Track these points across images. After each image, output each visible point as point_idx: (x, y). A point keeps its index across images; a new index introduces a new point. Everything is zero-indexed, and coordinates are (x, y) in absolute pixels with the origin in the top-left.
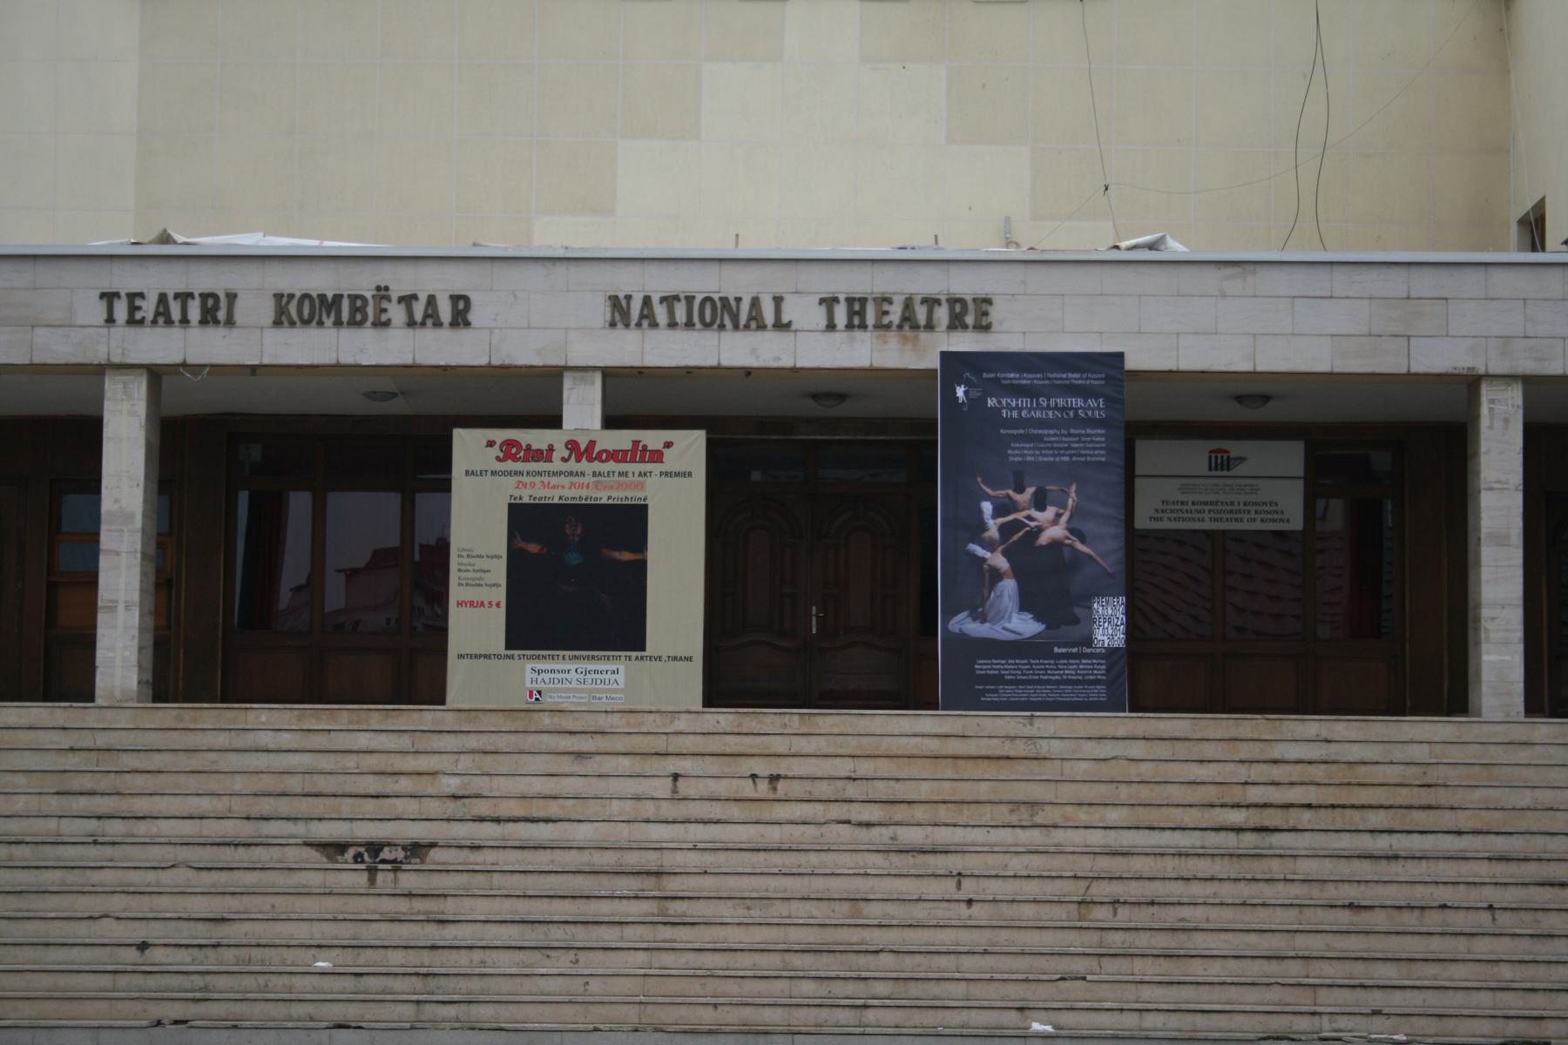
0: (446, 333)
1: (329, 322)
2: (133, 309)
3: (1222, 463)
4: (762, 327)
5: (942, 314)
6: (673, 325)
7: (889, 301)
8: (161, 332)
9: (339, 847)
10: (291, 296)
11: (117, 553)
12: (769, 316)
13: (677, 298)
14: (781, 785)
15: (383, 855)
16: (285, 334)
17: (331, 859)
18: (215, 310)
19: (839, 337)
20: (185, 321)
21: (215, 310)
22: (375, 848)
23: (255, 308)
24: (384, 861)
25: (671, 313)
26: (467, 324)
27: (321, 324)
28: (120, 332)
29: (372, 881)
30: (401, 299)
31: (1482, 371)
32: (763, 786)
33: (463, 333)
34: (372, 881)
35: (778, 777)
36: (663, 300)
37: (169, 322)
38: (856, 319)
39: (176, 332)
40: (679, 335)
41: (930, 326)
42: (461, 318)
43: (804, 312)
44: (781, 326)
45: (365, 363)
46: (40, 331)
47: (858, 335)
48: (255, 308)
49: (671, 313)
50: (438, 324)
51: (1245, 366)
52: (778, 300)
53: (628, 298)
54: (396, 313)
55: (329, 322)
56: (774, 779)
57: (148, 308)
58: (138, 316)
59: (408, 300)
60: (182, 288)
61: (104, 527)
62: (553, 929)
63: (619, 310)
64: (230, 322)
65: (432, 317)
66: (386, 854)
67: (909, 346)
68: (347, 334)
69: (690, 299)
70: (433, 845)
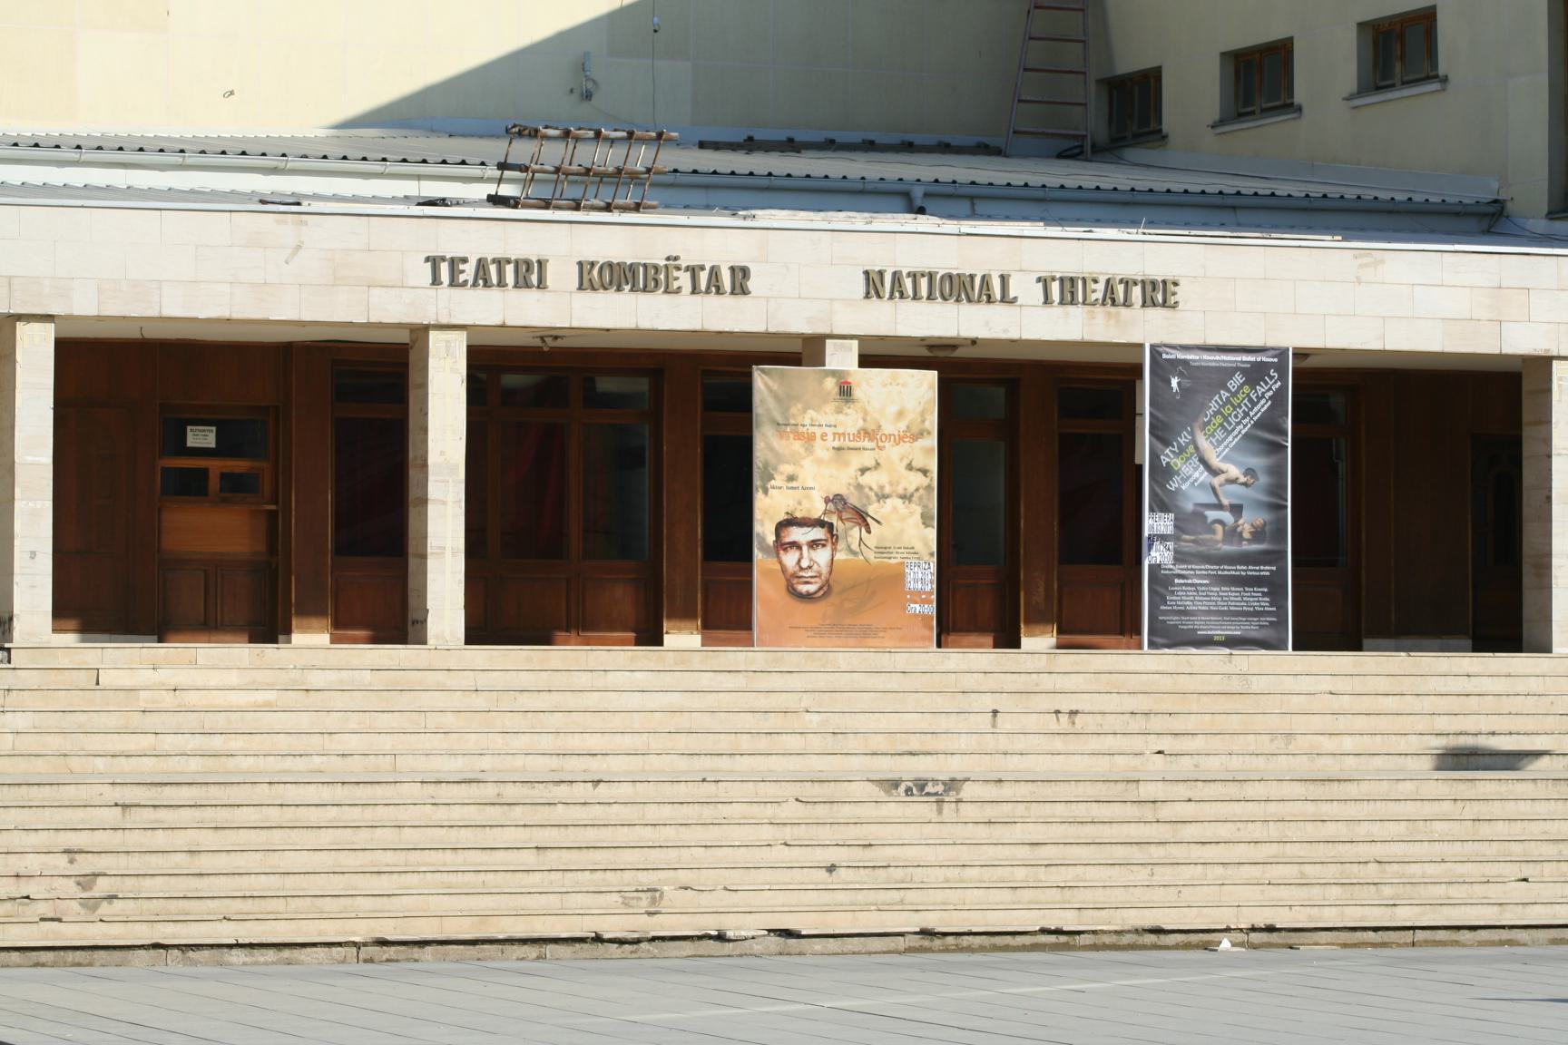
0: (727, 300)
1: (628, 288)
2: (454, 272)
3: (71, 862)
4: (990, 300)
5: (1136, 292)
6: (916, 297)
7: (465, 260)
8: (481, 292)
9: (895, 784)
10: (593, 264)
11: (444, 503)
12: (997, 294)
13: (443, 259)
14: (1078, 719)
15: (927, 789)
16: (588, 296)
17: (888, 792)
18: (529, 274)
19: (1057, 311)
20: (501, 283)
21: (529, 274)
22: (921, 785)
23: (562, 275)
24: (928, 794)
25: (501, 273)
26: (745, 292)
27: (619, 289)
28: (445, 291)
29: (940, 811)
30: (687, 269)
31: (1555, 353)
32: (1064, 718)
33: (742, 300)
34: (940, 811)
35: (1077, 712)
36: (909, 275)
37: (487, 284)
38: (1069, 298)
39: (495, 293)
40: (923, 307)
41: (1127, 303)
42: (740, 288)
43: (1025, 289)
44: (434, 262)
45: (201, 316)
46: (375, 291)
47: (1071, 308)
48: (562, 275)
49: (501, 273)
50: (719, 291)
51: (760, 328)
52: (1004, 279)
53: (881, 273)
54: (684, 280)
55: (628, 288)
56: (1073, 713)
57: (469, 271)
58: (462, 278)
59: (694, 271)
60: (499, 254)
61: (431, 478)
62: (1153, 848)
63: (873, 284)
64: (541, 285)
65: (715, 285)
66: (929, 788)
67: (1112, 322)
68: (643, 298)
69: (931, 276)
70: (967, 780)
